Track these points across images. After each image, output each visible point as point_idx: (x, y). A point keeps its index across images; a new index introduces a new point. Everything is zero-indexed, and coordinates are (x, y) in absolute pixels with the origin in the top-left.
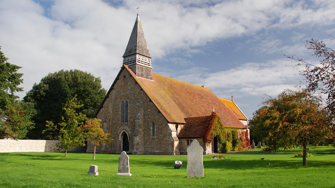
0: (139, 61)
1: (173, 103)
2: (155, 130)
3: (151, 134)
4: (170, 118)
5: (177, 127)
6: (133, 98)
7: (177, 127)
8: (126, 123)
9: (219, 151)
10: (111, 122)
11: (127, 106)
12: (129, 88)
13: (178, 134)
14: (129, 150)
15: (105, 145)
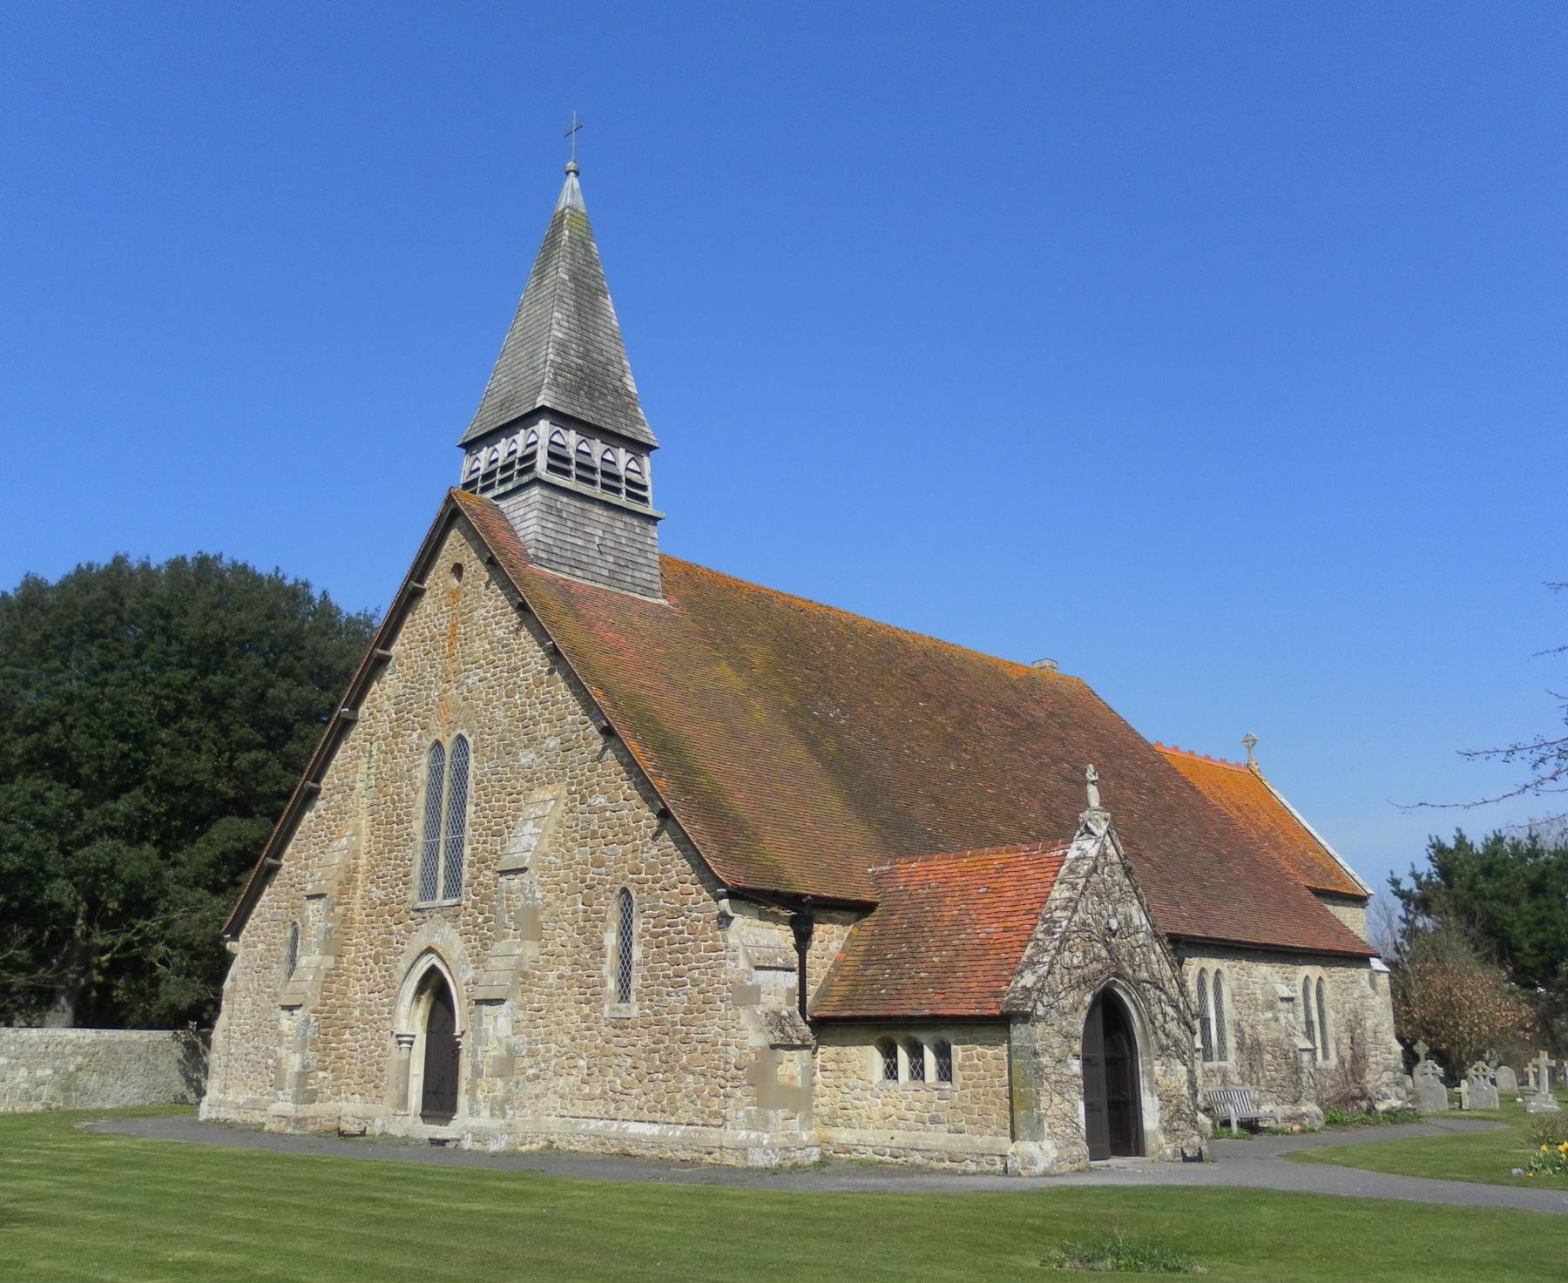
1: (798, 752)
2: (637, 953)
3: (604, 984)
4: (748, 859)
6: (499, 715)
8: (448, 902)
9: (1150, 1144)
10: (359, 892)
12: (479, 646)
13: (811, 989)
14: (453, 1108)
15: (297, 1068)
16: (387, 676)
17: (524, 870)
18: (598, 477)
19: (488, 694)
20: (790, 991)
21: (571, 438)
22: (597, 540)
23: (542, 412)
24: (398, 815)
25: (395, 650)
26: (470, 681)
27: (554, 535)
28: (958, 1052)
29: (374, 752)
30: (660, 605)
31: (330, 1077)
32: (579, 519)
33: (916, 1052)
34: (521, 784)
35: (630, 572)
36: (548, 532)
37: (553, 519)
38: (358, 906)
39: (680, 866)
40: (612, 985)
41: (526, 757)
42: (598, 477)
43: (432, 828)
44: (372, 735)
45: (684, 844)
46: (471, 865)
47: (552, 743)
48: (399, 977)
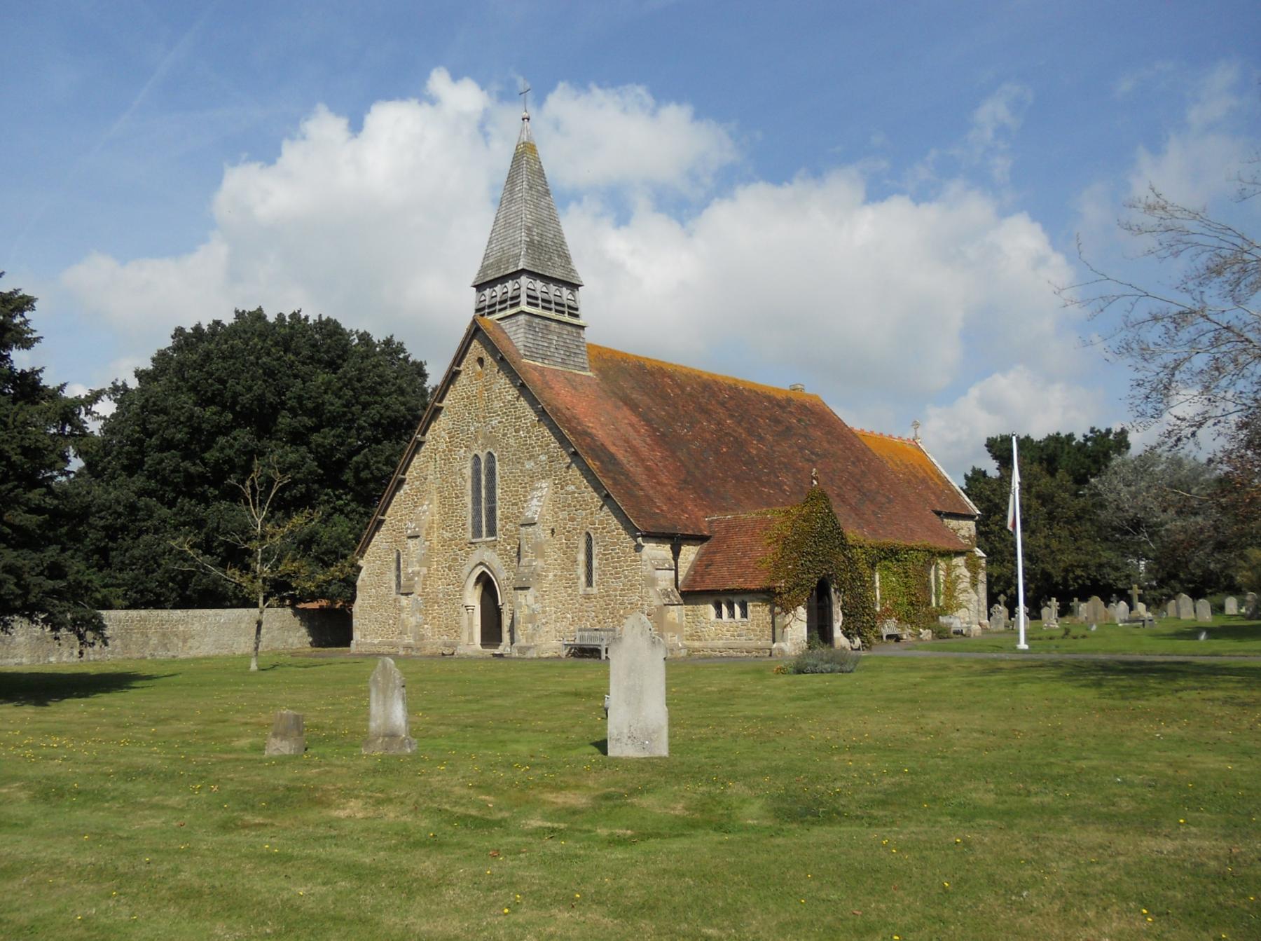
0: (544, 304)
2: (595, 563)
3: (578, 578)
5: (676, 554)
6: (512, 441)
7: (676, 554)
8: (489, 539)
11: (491, 473)
13: (680, 578)
16: (442, 417)
17: (535, 524)
18: (553, 306)
19: (504, 430)
20: (671, 579)
21: (539, 285)
22: (554, 342)
23: (523, 272)
24: (456, 494)
25: (445, 402)
26: (493, 423)
27: (532, 341)
28: (750, 607)
29: (438, 459)
30: (589, 376)
31: (430, 627)
32: (545, 332)
33: (731, 608)
34: (527, 479)
35: (572, 359)
36: (529, 340)
37: (532, 332)
38: (436, 542)
39: (614, 521)
40: (583, 579)
41: (529, 465)
42: (553, 306)
43: (477, 500)
44: (435, 450)
45: (617, 512)
46: (501, 520)
47: (543, 458)
48: (463, 577)
